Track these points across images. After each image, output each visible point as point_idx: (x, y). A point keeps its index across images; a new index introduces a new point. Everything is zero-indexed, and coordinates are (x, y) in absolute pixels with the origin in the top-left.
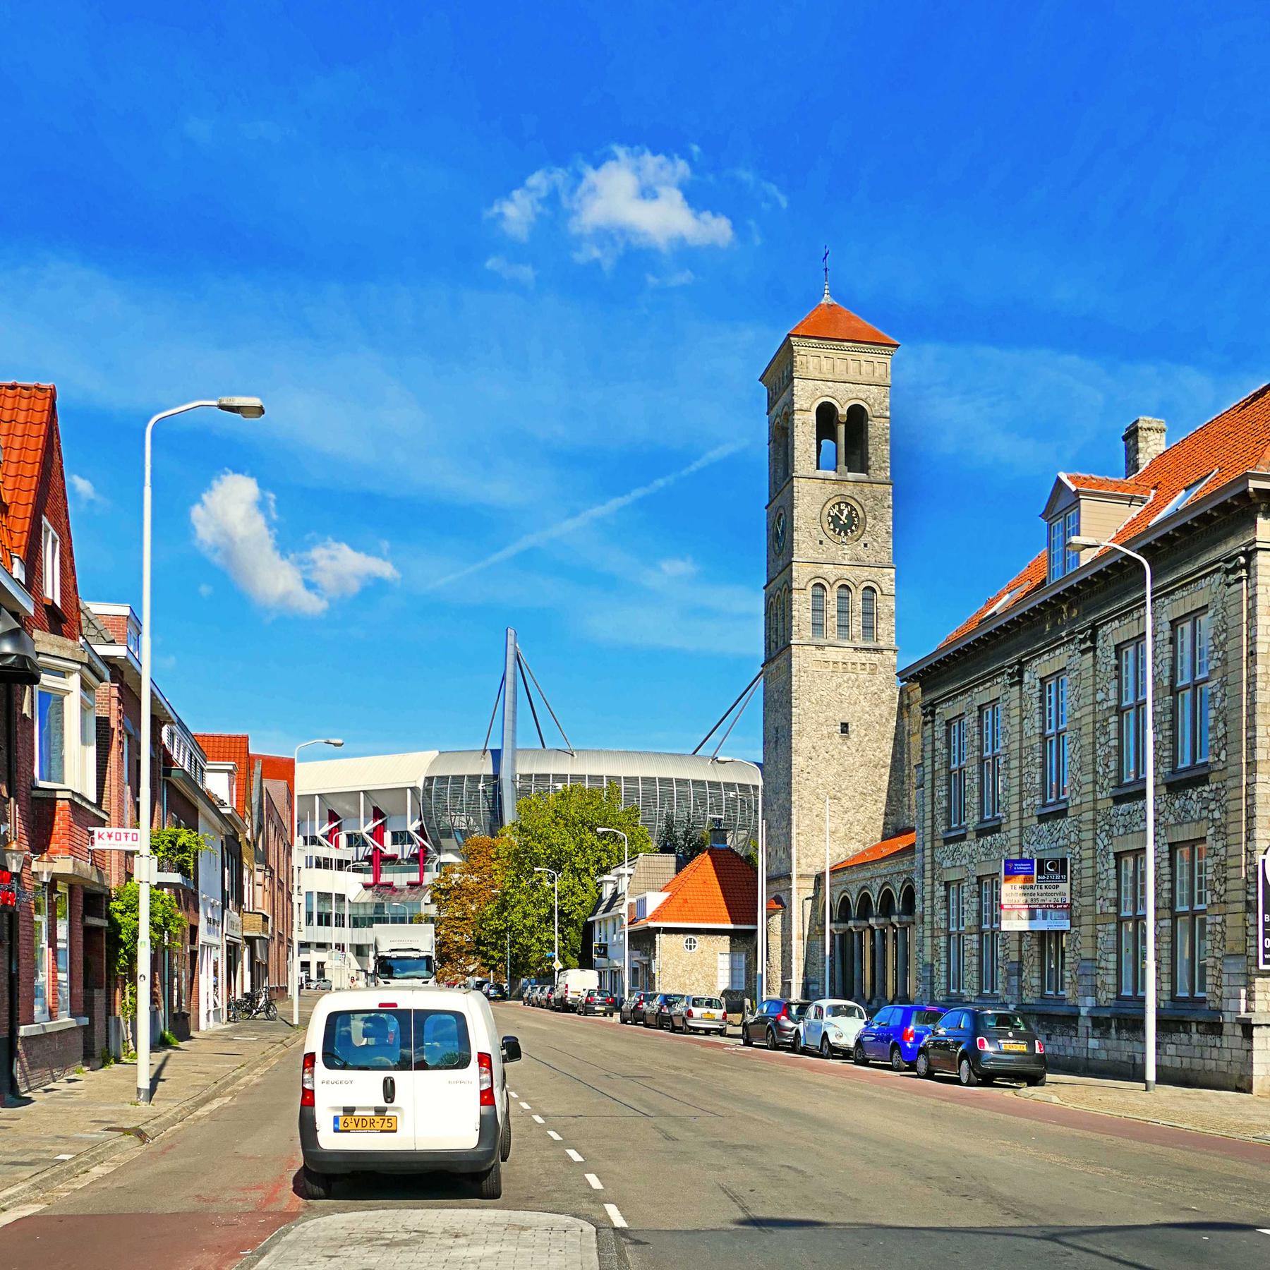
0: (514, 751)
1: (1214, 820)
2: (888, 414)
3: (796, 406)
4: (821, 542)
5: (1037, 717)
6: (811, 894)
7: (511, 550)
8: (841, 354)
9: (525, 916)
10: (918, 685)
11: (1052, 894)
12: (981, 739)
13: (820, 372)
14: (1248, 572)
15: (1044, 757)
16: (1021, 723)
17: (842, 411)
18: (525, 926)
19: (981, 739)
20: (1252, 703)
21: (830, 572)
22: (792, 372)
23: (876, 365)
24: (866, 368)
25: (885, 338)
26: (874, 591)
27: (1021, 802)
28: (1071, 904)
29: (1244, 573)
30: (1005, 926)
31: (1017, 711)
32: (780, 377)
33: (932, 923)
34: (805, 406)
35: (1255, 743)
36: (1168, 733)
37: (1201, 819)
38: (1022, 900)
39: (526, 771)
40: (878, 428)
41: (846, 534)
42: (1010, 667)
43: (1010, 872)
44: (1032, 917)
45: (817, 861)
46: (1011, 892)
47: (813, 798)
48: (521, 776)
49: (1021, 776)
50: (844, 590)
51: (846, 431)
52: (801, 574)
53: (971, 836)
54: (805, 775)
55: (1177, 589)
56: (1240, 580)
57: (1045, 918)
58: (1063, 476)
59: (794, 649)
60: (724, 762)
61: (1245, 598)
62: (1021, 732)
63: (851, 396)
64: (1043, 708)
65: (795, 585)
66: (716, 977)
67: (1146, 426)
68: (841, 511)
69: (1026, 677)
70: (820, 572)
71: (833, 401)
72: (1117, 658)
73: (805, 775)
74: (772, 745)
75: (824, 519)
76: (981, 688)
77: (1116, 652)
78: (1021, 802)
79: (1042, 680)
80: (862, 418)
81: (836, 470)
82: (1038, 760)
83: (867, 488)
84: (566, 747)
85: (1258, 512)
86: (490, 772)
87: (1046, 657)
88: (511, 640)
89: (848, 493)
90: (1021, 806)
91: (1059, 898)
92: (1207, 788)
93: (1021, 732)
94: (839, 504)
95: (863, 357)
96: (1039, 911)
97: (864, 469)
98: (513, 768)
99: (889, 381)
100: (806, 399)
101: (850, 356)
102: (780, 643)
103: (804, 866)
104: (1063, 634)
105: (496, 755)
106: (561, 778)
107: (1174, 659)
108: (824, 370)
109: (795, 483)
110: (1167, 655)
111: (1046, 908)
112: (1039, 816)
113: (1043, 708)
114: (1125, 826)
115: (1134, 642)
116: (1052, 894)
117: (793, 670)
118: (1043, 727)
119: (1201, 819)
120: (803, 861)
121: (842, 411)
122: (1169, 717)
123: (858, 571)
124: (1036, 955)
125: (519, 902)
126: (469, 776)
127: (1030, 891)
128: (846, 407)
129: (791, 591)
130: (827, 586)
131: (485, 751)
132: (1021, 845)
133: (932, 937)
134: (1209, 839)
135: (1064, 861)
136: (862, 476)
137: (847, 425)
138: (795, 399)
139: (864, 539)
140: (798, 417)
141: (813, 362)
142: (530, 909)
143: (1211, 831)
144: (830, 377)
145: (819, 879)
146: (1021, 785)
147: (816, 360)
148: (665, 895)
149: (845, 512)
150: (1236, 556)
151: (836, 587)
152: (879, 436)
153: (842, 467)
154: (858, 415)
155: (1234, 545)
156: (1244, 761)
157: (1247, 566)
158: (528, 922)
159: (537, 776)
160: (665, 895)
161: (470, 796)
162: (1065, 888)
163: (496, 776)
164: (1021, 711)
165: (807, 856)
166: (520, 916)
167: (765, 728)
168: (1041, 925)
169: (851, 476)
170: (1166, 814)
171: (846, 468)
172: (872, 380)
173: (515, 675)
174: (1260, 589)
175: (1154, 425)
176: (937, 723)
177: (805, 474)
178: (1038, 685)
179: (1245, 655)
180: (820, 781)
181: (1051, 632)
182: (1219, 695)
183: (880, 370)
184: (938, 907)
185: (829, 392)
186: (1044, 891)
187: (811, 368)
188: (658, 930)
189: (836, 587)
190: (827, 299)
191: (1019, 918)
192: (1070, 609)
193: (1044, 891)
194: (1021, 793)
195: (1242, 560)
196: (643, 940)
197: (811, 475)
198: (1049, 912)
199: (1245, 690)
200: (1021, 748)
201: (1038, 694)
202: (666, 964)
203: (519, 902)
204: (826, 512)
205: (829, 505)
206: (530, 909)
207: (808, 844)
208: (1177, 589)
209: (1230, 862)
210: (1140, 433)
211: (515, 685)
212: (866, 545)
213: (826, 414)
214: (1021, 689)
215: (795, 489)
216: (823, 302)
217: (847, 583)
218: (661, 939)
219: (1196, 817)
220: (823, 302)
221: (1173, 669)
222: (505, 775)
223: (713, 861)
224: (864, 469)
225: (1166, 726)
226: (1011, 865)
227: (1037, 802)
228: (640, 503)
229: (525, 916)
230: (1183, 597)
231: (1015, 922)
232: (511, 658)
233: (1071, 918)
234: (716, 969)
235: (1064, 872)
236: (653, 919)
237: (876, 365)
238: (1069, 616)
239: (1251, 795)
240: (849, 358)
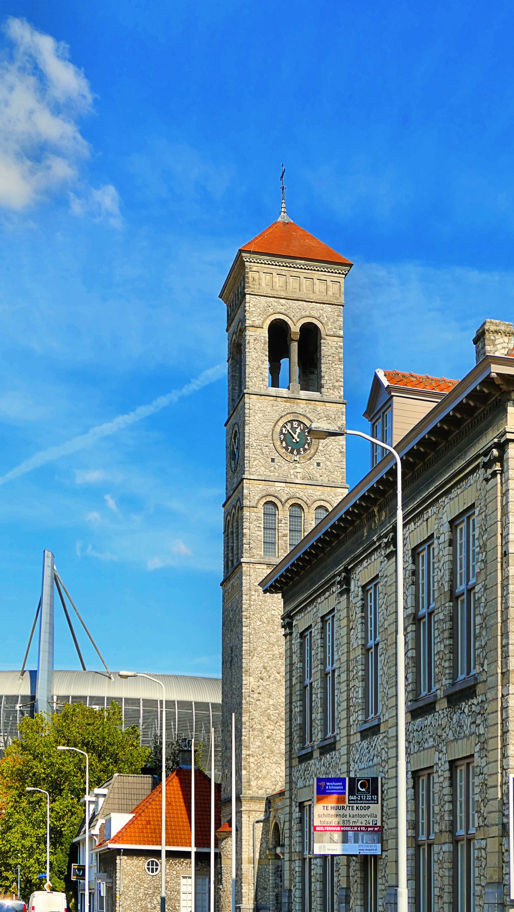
0: (51, 672)
1: (479, 735)
2: (341, 333)
3: (248, 323)
4: (273, 460)
5: (359, 627)
6: (262, 817)
7: (26, 467)
8: (295, 272)
9: (24, 836)
10: (280, 595)
11: (364, 816)
12: (325, 652)
13: (273, 289)
14: (502, 466)
15: (366, 670)
16: (348, 634)
17: (295, 328)
18: (23, 846)
19: (325, 652)
20: (506, 608)
21: (281, 490)
22: (244, 288)
23: (330, 283)
24: (319, 286)
25: (340, 258)
26: (300, 506)
27: (348, 718)
28: (382, 827)
29: (497, 467)
30: (318, 849)
31: (344, 622)
32: (235, 293)
33: (290, 845)
34: (257, 323)
35: (507, 652)
36: (447, 642)
37: (471, 734)
38: (335, 821)
39: (63, 693)
40: (331, 348)
41: (299, 453)
42: (339, 574)
43: (323, 792)
44: (345, 840)
45: (268, 783)
46: (324, 813)
47: (264, 719)
48: (58, 697)
49: (348, 690)
50: (271, 507)
51: (297, 350)
52: (252, 492)
53: (316, 754)
54: (256, 696)
55: (452, 487)
56: (494, 474)
57: (356, 842)
58: (381, 375)
59: (245, 567)
60: (126, 677)
61: (499, 494)
62: (348, 643)
63: (304, 314)
64: (365, 618)
65: (246, 502)
66: (179, 900)
67: (493, 328)
68: (294, 429)
69: (352, 588)
70: (271, 490)
71: (286, 319)
72: (414, 563)
73: (256, 696)
74: (228, 665)
75: (276, 436)
76: (323, 598)
77: (413, 556)
78: (348, 718)
79: (363, 587)
80: (317, 334)
81: (289, 388)
82: (360, 673)
83: (320, 407)
84: (103, 670)
85: (509, 400)
86: (27, 692)
87: (365, 564)
88: (48, 561)
89: (300, 411)
90: (348, 722)
91: (371, 819)
92: (475, 701)
93: (348, 643)
94: (291, 421)
95: (316, 275)
96: (351, 834)
97: (319, 388)
98: (49, 690)
99: (342, 300)
100: (258, 316)
101: (302, 274)
102: (235, 564)
103: (254, 789)
104: (375, 538)
105: (34, 675)
106: (99, 700)
107: (454, 562)
108: (277, 286)
109: (247, 400)
110: (447, 558)
111: (358, 830)
112: (361, 732)
113: (365, 618)
114: (419, 743)
115: (426, 546)
116: (364, 816)
117: (244, 588)
118: (366, 638)
119: (471, 734)
120: (253, 783)
121: (295, 328)
122: (448, 625)
123: (310, 490)
124: (359, 881)
125: (18, 822)
126: (7, 697)
127: (342, 812)
128: (299, 325)
129: (241, 508)
130: (279, 504)
131: (23, 672)
132: (348, 763)
133: (290, 860)
134: (476, 755)
135: (375, 779)
136: (315, 395)
137: (300, 342)
138: (247, 315)
139: (317, 458)
140: (249, 333)
141: (265, 279)
142: (28, 830)
143: (477, 748)
144: (283, 294)
145: (269, 801)
146: (348, 699)
147: (268, 277)
148: (131, 816)
149: (298, 430)
150: (490, 449)
151: (288, 505)
152: (333, 355)
153: (296, 384)
154: (311, 334)
155: (491, 437)
156: (499, 671)
157: (501, 459)
158: (27, 843)
159: (73, 697)
160: (131, 816)
161: (7, 717)
162: (375, 809)
163: (33, 698)
164: (349, 621)
165: (257, 778)
166: (18, 836)
167: (223, 648)
168: (354, 849)
169: (303, 394)
170: (447, 730)
171: (298, 386)
172: (325, 299)
173: (52, 597)
174: (512, 484)
175: (503, 328)
176: (294, 635)
177: (257, 391)
178: (360, 593)
179: (499, 556)
180: (271, 702)
181: (368, 537)
182: (483, 600)
183: (334, 289)
184: (294, 829)
185: (314, 313)
186: (356, 812)
187: (263, 284)
188: (118, 852)
189: (288, 505)
190: (283, 218)
191: (332, 841)
192: (379, 511)
193: (356, 812)
194: (348, 708)
195: (495, 452)
196: (108, 861)
197: (263, 392)
198: (361, 834)
199: (499, 594)
200: (348, 661)
201: (360, 603)
202: (127, 887)
203: (18, 822)
204: (278, 429)
205: (281, 423)
206: (28, 830)
207: (259, 766)
208: (452, 487)
209: (490, 783)
210: (487, 336)
211: (52, 606)
212: (318, 464)
213: (278, 331)
214: (348, 598)
215: (247, 406)
216: (279, 219)
217: (299, 502)
218: (122, 861)
219: (467, 732)
220: (279, 219)
221: (453, 573)
222: (41, 696)
223: (181, 783)
224: (319, 388)
225: (446, 634)
226: (323, 784)
227: (360, 718)
228: (153, 422)
229: (24, 836)
230: (458, 495)
231: (329, 845)
232: (47, 581)
233: (382, 841)
234: (179, 893)
235: (375, 792)
236: (114, 841)
237: (327, 284)
238: (380, 519)
239: (505, 708)
240: (329, 279)
